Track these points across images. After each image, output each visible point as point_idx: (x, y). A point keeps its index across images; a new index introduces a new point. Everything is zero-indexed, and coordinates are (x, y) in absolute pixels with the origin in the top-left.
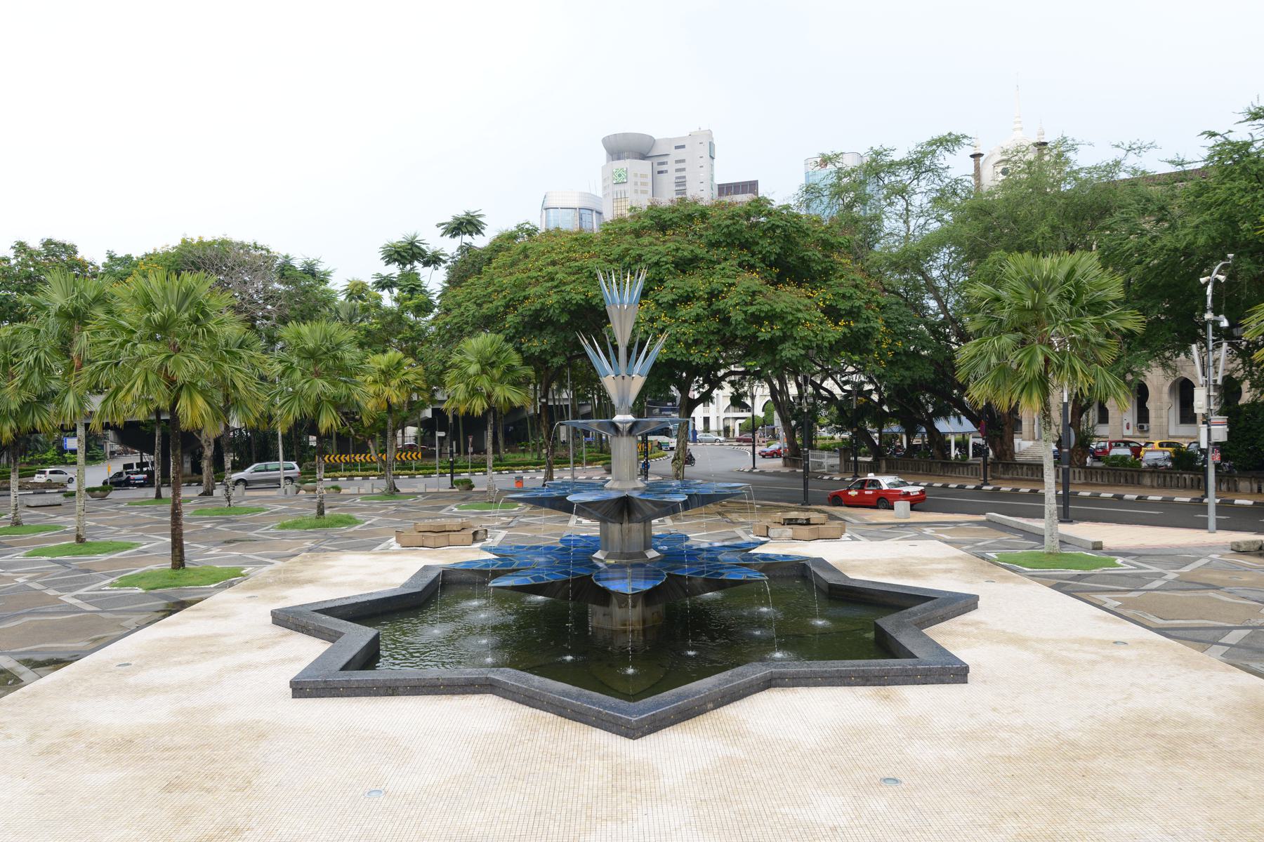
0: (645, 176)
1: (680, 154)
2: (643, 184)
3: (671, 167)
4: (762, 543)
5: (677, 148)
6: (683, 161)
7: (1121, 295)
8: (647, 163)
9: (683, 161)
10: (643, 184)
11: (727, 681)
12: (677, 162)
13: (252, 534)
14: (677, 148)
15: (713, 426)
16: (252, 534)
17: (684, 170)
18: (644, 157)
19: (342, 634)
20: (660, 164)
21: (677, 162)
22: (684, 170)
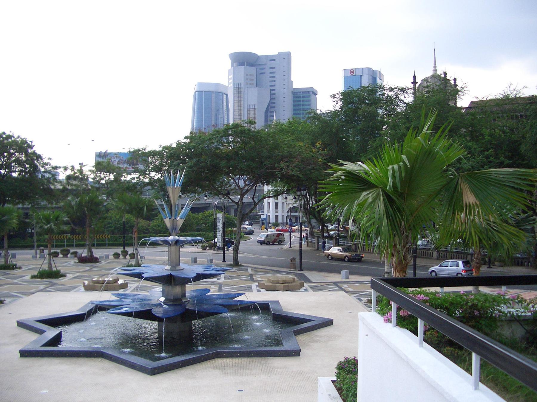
0: (253, 75)
1: (273, 64)
2: (251, 80)
3: (268, 71)
4: (241, 295)
5: (271, 60)
6: (274, 68)
7: (232, 263)
8: (255, 68)
9: (274, 68)
10: (251, 80)
11: (240, 348)
12: (271, 68)
13: (15, 281)
14: (271, 60)
15: (280, 221)
16: (15, 281)
17: (274, 72)
18: (251, 65)
19: (471, 375)
20: (261, 69)
21: (271, 68)
22: (274, 72)
